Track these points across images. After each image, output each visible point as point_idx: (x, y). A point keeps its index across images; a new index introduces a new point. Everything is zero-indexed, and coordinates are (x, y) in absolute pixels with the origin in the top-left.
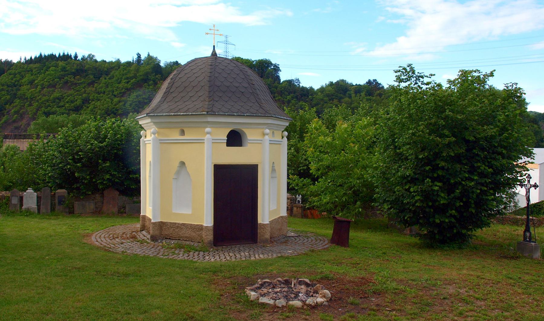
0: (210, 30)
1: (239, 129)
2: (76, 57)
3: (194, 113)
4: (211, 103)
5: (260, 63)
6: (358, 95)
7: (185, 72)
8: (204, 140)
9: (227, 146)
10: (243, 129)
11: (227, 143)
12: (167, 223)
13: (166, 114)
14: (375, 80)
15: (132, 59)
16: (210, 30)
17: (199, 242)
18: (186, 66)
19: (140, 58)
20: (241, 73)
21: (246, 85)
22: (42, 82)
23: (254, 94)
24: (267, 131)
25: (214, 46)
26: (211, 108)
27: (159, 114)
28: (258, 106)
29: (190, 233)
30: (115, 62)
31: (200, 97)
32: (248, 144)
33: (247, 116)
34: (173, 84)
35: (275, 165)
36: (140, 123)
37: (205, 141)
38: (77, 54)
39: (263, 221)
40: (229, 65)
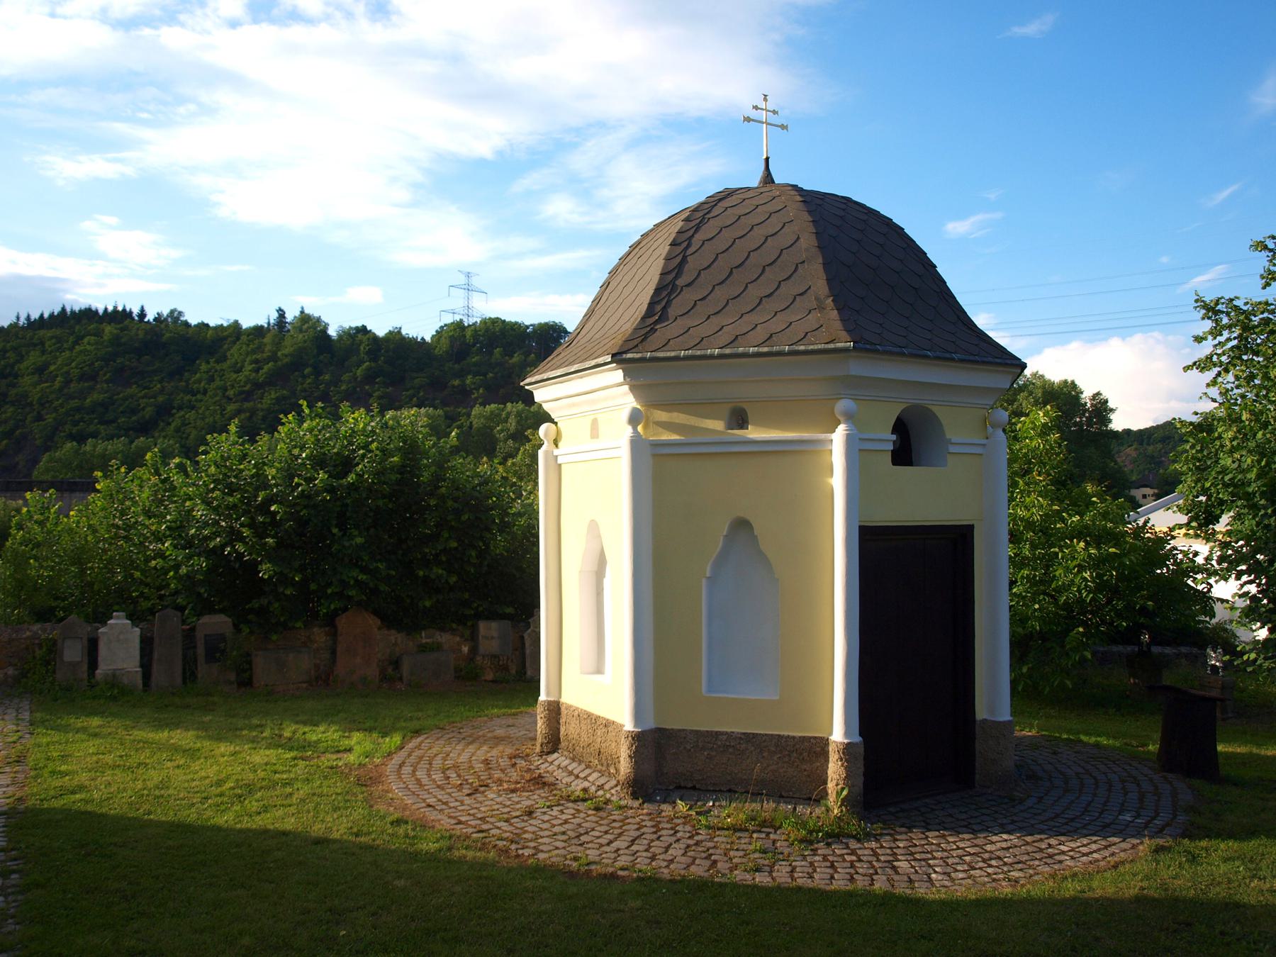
2: (142, 314)
15: (267, 321)
19: (285, 318)
22: (65, 369)
30: (229, 326)
38: (145, 308)
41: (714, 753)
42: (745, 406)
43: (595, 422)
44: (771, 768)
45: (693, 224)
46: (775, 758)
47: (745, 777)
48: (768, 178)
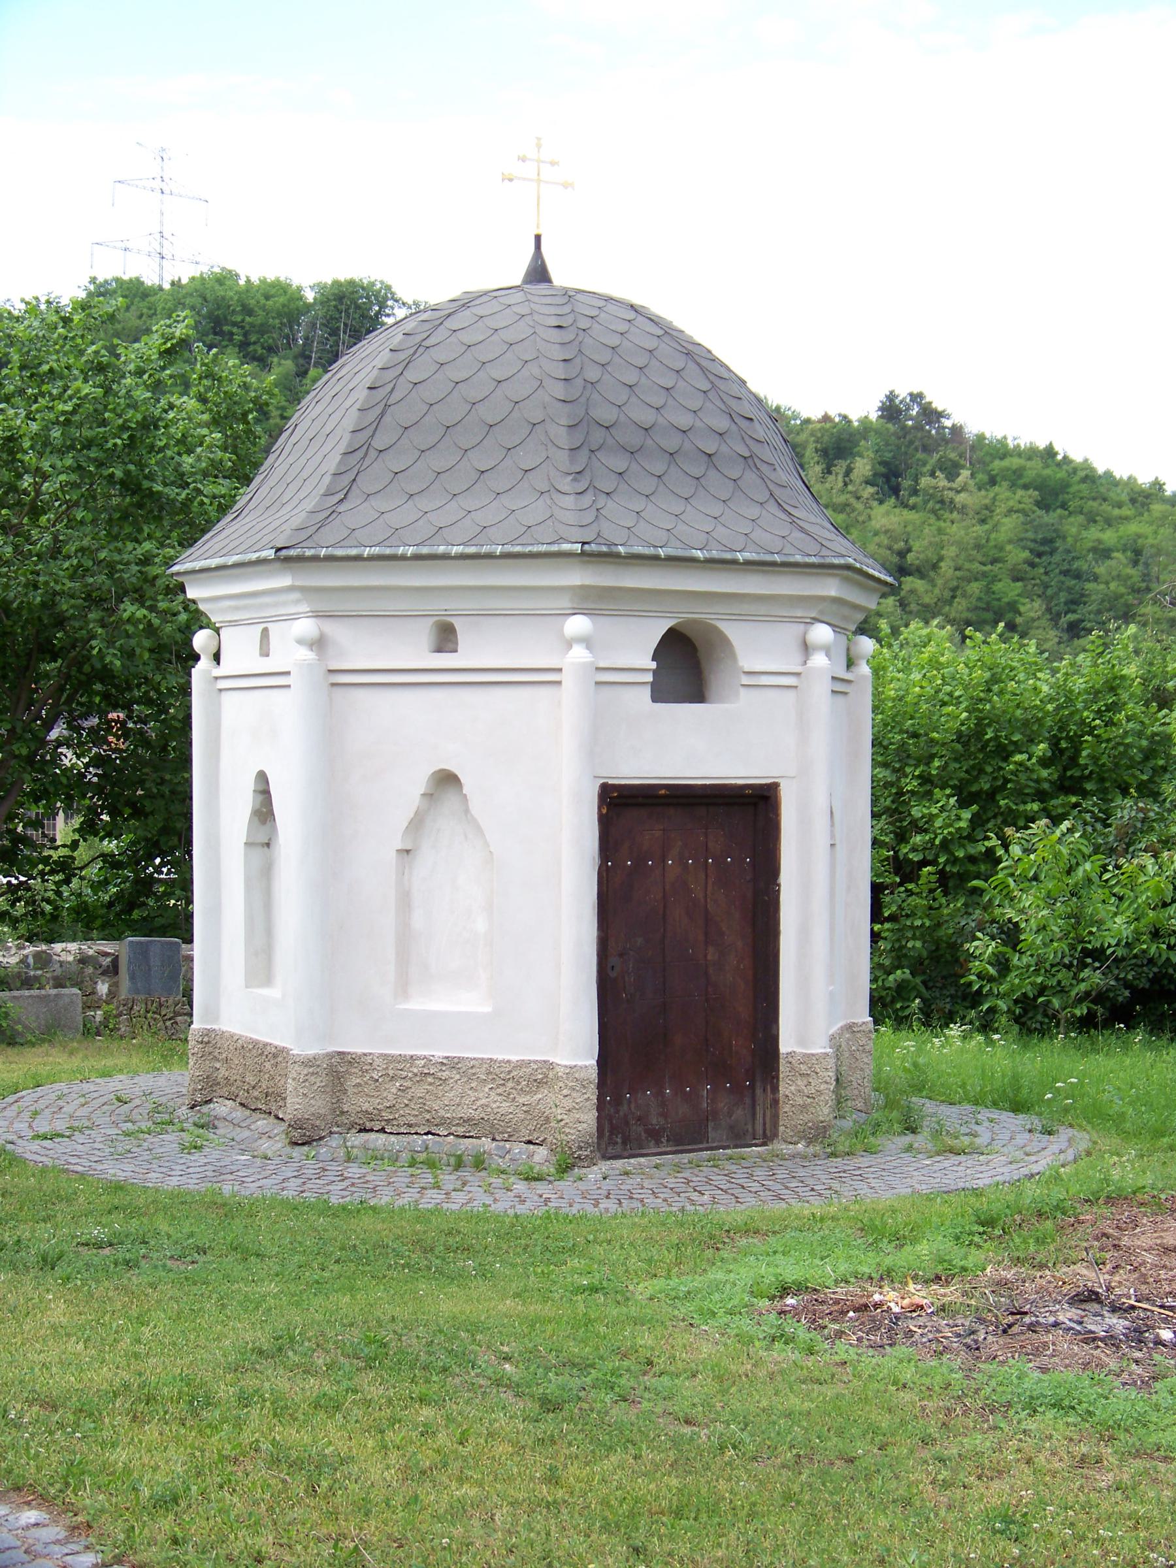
0: (523, 159)
1: (695, 621)
3: (518, 549)
4: (587, 500)
5: (340, 298)
6: (840, 467)
8: (560, 670)
9: (655, 699)
11: (654, 686)
13: (376, 550)
14: (916, 397)
16: (523, 159)
17: (530, 1142)
20: (691, 365)
21: (722, 424)
23: (756, 460)
25: (538, 238)
27: (339, 552)
28: (783, 516)
29: (484, 1101)
31: (530, 475)
32: (742, 691)
34: (382, 414)
36: (191, 593)
37: (564, 677)
39: (802, 1042)
40: (633, 329)
41: (408, 1084)
42: (453, 620)
43: (265, 631)
44: (479, 1103)
45: (402, 356)
46: (487, 1090)
47: (448, 1115)
48: (539, 273)
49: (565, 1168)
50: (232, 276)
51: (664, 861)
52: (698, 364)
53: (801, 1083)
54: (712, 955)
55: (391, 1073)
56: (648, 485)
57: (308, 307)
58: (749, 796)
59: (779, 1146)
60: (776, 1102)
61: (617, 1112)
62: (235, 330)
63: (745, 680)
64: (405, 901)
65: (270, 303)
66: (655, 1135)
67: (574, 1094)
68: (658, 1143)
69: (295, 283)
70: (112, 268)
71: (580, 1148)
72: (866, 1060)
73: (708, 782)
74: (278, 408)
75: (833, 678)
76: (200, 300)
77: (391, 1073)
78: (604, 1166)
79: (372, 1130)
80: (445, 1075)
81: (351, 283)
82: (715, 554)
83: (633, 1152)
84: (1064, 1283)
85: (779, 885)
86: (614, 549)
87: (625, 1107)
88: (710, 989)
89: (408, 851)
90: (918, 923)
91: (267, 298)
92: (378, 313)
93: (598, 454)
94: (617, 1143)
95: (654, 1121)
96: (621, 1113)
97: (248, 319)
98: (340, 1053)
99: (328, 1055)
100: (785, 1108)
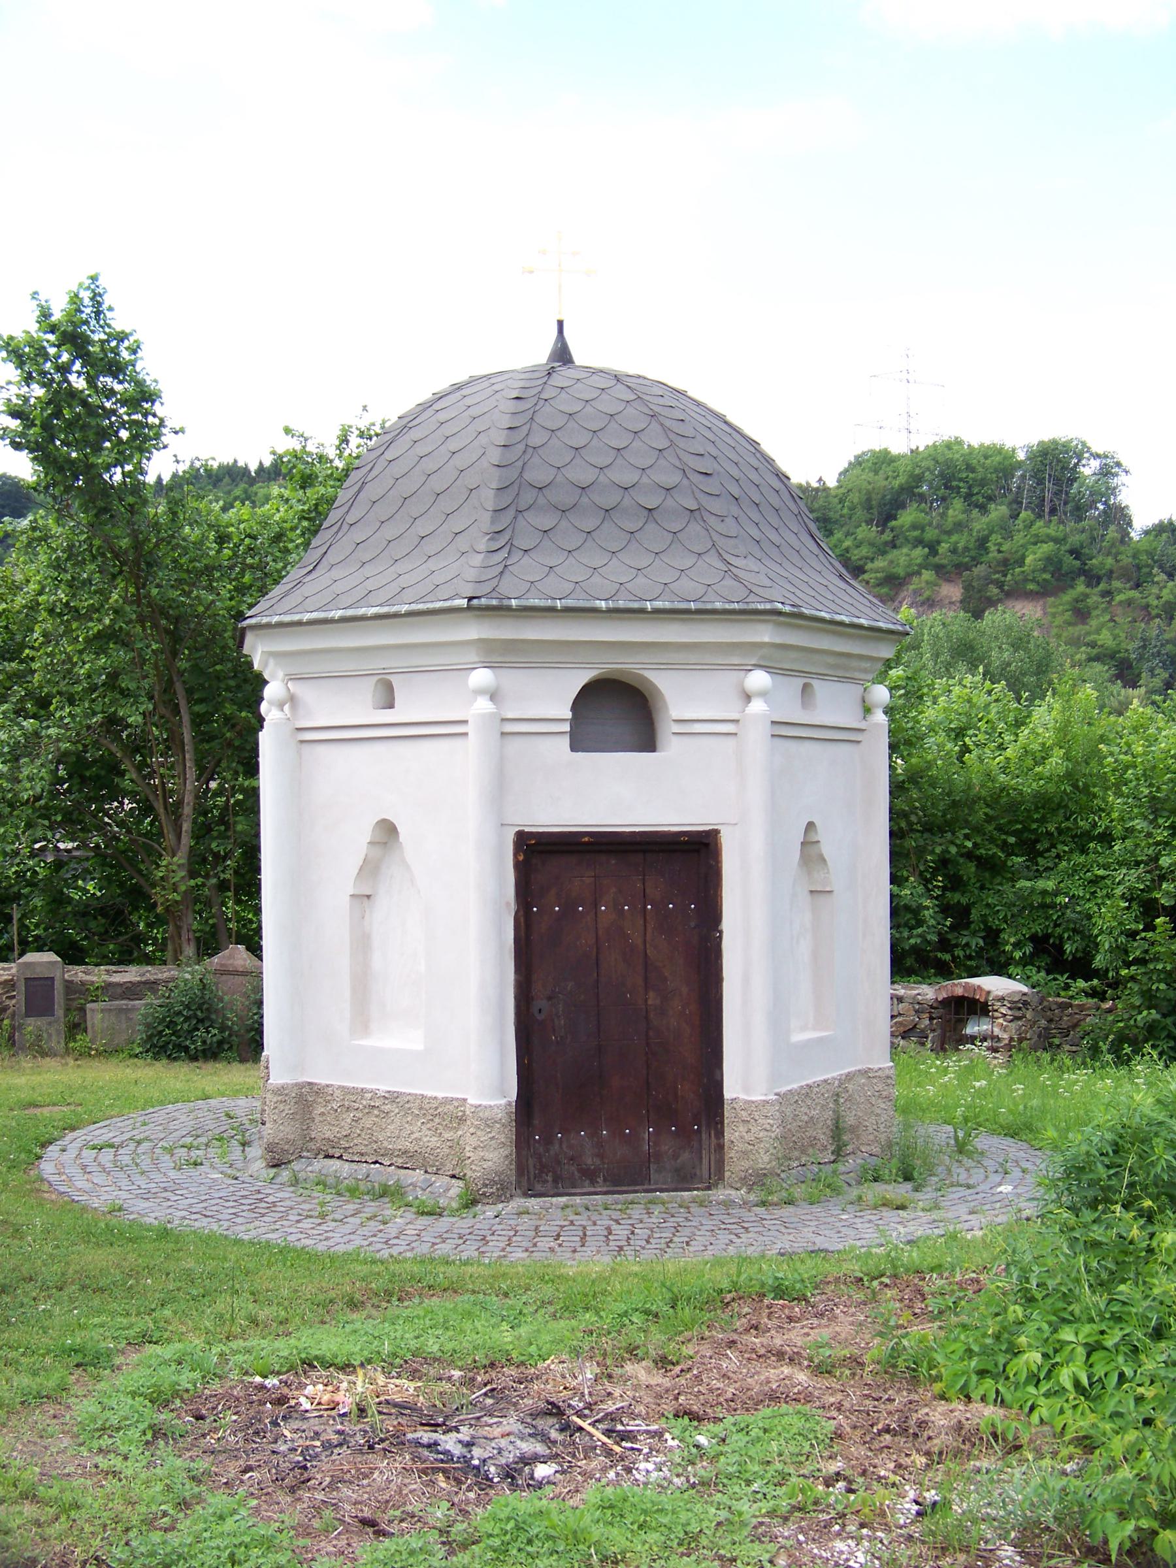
7: (415, 434)
9: (574, 748)
10: (647, 674)
12: (330, 1091)
13: (315, 615)
17: (453, 1176)
18: (424, 410)
20: (655, 426)
24: (759, 679)
25: (560, 324)
26: (495, 582)
32: (675, 739)
33: (657, 611)
34: (359, 491)
35: (821, 835)
41: (359, 1115)
44: (413, 1136)
46: (419, 1124)
48: (562, 355)
49: (471, 1202)
50: (959, 442)
51: (596, 906)
52: (662, 425)
53: (742, 1129)
54: (653, 999)
55: (346, 1103)
56: (575, 541)
57: (1020, 464)
58: (686, 843)
59: (720, 1194)
60: (720, 1147)
61: (548, 1151)
62: (961, 484)
63: (676, 728)
64: (362, 944)
65: (988, 461)
66: (590, 1175)
67: (479, 1133)
68: (593, 1182)
69: (1009, 445)
70: (873, 442)
71: (486, 1185)
72: (883, 1106)
73: (637, 829)
74: (995, 545)
75: (773, 722)
76: (933, 463)
77: (346, 1103)
78: (519, 1203)
79: (333, 1157)
80: (387, 1108)
81: (1054, 442)
82: (621, 604)
83: (567, 1191)
84: (565, 1388)
85: (721, 932)
86: (506, 602)
87: (557, 1146)
88: (651, 1033)
89: (368, 897)
90: (1160, 966)
91: (986, 457)
92: (1076, 465)
93: (525, 514)
94: (546, 1181)
95: (589, 1161)
96: (552, 1152)
97: (971, 475)
98: (310, 1084)
99: (296, 1084)
100: (731, 1154)
